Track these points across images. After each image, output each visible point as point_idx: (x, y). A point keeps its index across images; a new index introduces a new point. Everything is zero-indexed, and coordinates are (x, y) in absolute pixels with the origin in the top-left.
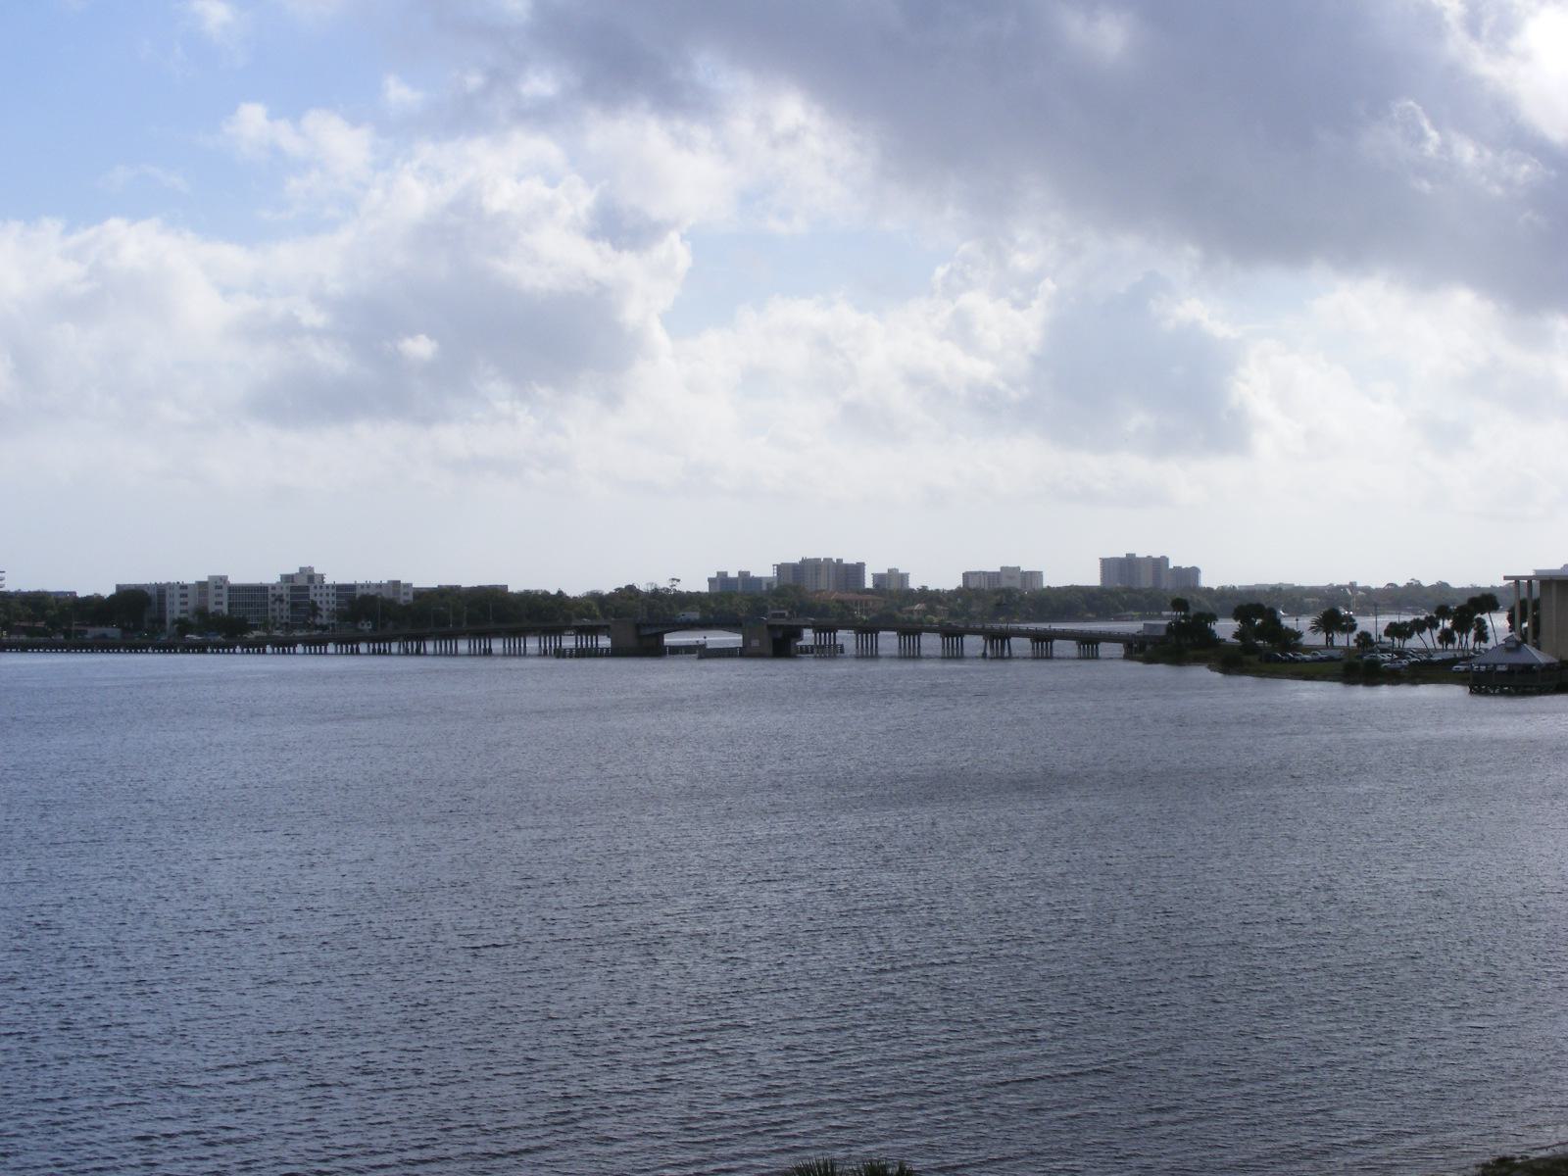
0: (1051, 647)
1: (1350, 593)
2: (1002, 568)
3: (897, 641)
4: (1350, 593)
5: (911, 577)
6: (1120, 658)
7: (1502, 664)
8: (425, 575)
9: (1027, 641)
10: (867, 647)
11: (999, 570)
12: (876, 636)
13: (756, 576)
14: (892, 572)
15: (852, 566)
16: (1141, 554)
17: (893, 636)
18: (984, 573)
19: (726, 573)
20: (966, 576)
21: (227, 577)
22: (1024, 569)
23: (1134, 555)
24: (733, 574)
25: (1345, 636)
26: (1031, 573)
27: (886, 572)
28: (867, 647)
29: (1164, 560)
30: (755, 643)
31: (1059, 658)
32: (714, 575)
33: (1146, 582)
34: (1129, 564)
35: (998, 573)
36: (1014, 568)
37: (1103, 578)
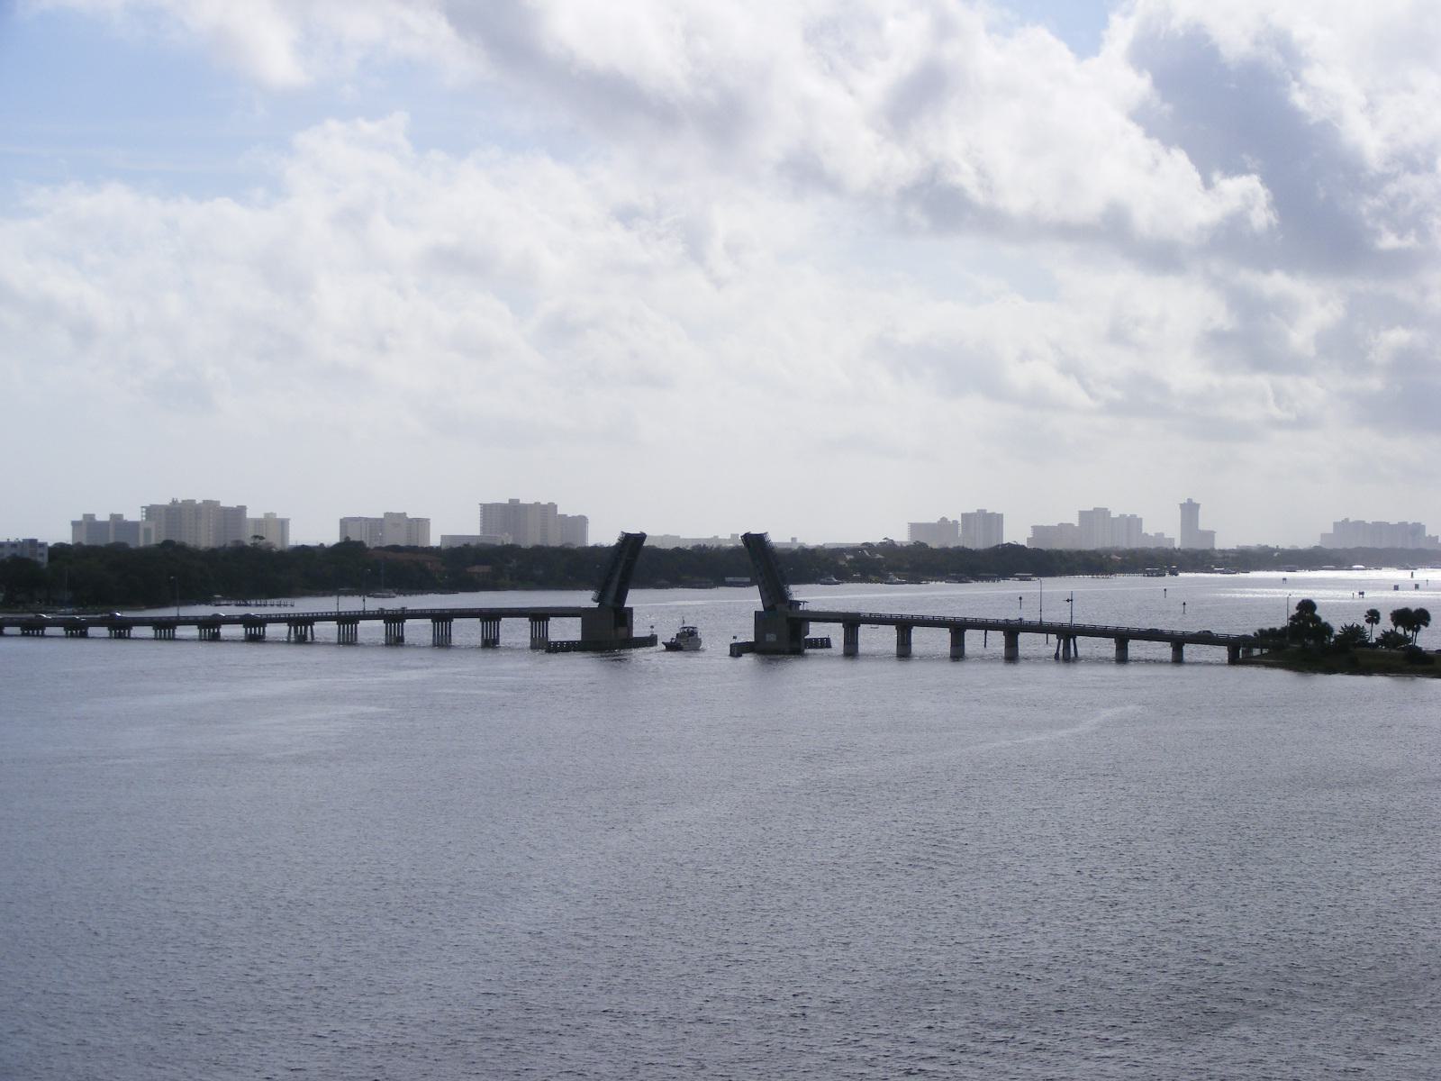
0: (356, 629)
1: (867, 554)
2: (386, 514)
3: (480, 624)
4: (867, 554)
5: (291, 523)
6: (382, 645)
7: (277, 642)
8: (1285, 544)
9: (333, 625)
10: (438, 634)
11: (382, 516)
12: (498, 624)
13: (129, 520)
14: (272, 513)
15: (232, 510)
16: (525, 499)
17: (425, 626)
18: (366, 519)
19: (121, 515)
20: (345, 523)
21: (94, 515)
22: (410, 516)
23: (518, 500)
24: (102, 516)
25: (1074, 622)
26: (418, 520)
27: (262, 517)
28: (438, 634)
29: (553, 507)
30: (771, 637)
31: (1138, 661)
32: (79, 518)
33: (530, 539)
34: (510, 512)
35: (381, 520)
36: (399, 515)
37: (483, 528)
